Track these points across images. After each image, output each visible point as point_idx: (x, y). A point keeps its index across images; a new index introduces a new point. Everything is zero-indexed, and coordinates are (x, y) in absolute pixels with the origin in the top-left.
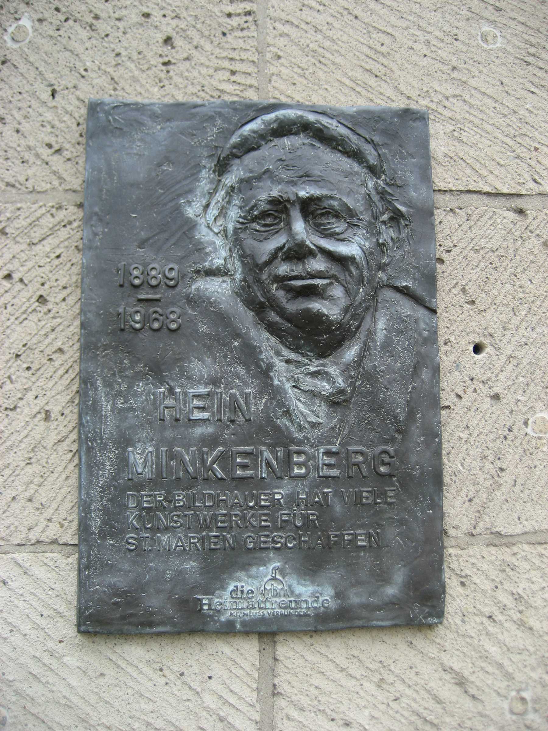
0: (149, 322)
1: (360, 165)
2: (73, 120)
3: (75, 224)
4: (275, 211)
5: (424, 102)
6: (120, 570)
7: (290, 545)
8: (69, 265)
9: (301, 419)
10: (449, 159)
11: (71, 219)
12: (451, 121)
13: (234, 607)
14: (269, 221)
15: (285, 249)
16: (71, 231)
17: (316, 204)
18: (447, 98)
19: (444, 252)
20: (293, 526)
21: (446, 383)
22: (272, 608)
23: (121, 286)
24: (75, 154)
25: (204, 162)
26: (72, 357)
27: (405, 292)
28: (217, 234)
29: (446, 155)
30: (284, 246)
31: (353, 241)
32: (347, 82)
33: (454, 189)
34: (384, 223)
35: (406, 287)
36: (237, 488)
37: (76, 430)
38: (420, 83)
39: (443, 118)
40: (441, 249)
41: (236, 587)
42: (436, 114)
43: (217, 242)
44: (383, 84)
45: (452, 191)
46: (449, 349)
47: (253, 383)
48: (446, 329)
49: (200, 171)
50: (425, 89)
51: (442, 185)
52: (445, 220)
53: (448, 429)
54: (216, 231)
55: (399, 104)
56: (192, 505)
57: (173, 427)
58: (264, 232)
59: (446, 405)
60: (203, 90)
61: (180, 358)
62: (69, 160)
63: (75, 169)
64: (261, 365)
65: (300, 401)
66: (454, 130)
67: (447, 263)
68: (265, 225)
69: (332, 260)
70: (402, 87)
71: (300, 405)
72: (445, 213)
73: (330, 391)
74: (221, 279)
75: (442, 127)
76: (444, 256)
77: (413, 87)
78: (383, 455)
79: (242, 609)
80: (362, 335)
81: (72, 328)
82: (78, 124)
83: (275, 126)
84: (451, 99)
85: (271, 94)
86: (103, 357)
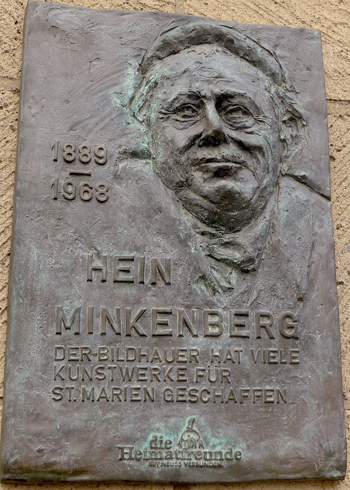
0: (79, 194)
1: (264, 72)
2: (12, 19)
3: (11, 107)
4: (193, 105)
5: (316, 27)
6: (45, 419)
7: (204, 399)
8: (4, 142)
9: (215, 283)
10: (338, 74)
11: (8, 102)
12: (339, 43)
13: (154, 457)
14: (187, 113)
15: (202, 137)
16: (7, 113)
17: (229, 101)
18: (336, 25)
19: (335, 151)
20: (207, 381)
21: (339, 262)
22: (188, 459)
23: (55, 160)
24: (12, 47)
25: (130, 62)
26: (4, 223)
27: (302, 180)
28: (141, 122)
29: (335, 71)
30: (201, 134)
31: (260, 134)
32: (252, 5)
33: (342, 99)
34: (284, 122)
35: (304, 177)
36: (156, 344)
37: (6, 289)
38: (313, 11)
39: (332, 40)
40: (333, 148)
41: (156, 437)
42: (326, 37)
43: (142, 129)
44: (281, 9)
45: (341, 100)
46: (341, 233)
47: (172, 251)
48: (338, 216)
49: (127, 68)
50: (317, 16)
51: (333, 96)
52: (335, 125)
53: (342, 302)
54: (141, 119)
55: (296, 25)
56: (115, 359)
57: (99, 287)
58: (184, 122)
59: (340, 281)
60: (127, 3)
61: (108, 227)
62: (6, 52)
63: (12, 60)
64: (180, 236)
65: (214, 268)
66: (342, 51)
67: (337, 160)
68: (184, 116)
69: (242, 149)
70: (298, 14)
71: (215, 273)
72: (335, 118)
73: (241, 259)
74: (144, 161)
75: (331, 48)
76: (335, 154)
77: (307, 14)
78: (287, 320)
79: (161, 459)
80: (267, 214)
81: (5, 197)
82: (16, 23)
83: (193, 34)
84: (339, 26)
85: (186, 11)
86: (37, 222)
